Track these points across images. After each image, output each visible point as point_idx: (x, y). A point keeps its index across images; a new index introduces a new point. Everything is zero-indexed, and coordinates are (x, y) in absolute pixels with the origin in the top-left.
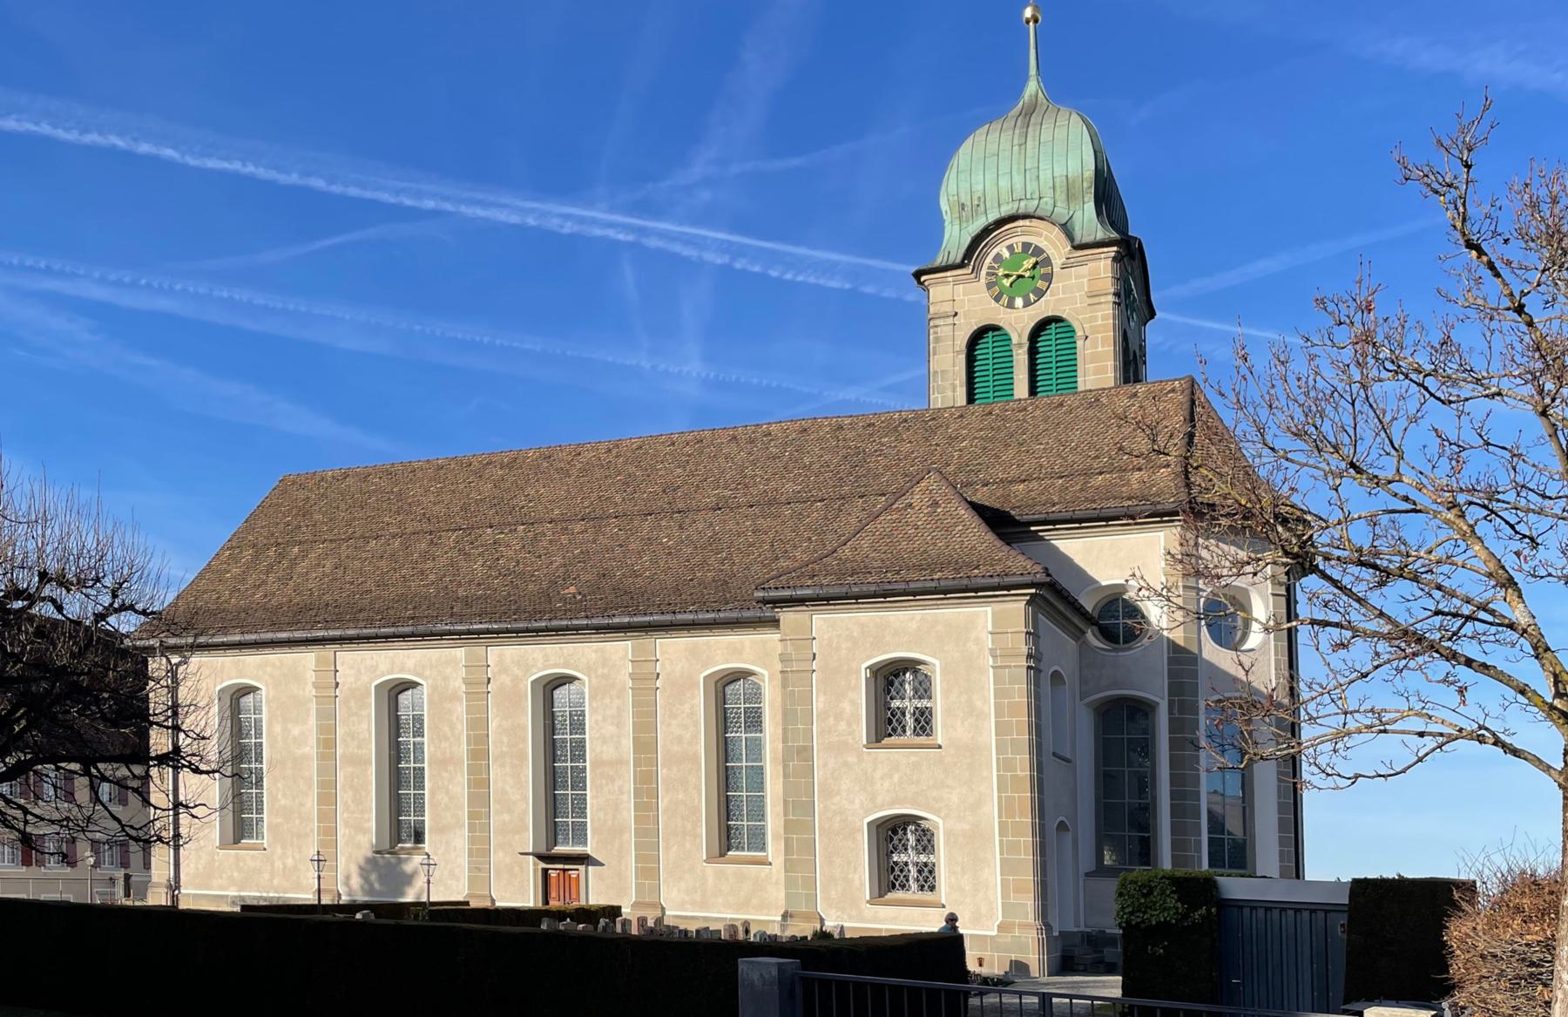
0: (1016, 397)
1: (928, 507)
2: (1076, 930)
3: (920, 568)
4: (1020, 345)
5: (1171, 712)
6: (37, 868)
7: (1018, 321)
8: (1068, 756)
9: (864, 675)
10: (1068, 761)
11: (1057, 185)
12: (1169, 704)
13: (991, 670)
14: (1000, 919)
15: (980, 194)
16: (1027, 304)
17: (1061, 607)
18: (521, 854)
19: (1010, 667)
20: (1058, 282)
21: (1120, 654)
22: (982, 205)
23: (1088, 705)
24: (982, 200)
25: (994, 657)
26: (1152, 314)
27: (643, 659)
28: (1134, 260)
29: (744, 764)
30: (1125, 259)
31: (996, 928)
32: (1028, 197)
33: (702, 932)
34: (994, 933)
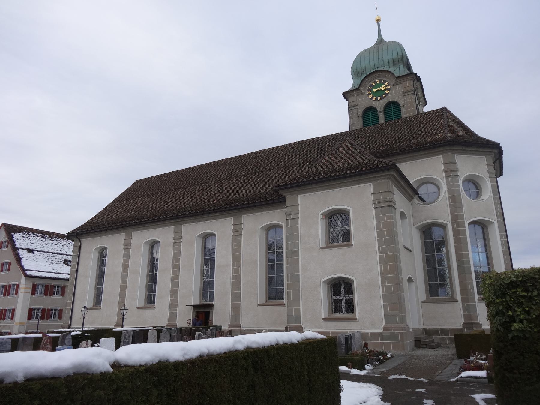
0: (380, 123)
1: (346, 151)
2: (419, 328)
3: (342, 170)
4: (381, 112)
5: (453, 227)
6: (47, 320)
7: (380, 105)
8: (410, 248)
9: (320, 217)
10: (410, 251)
11: (390, 61)
12: (452, 223)
13: (374, 210)
14: (384, 324)
15: (364, 68)
16: (382, 98)
17: (402, 183)
18: (187, 306)
19: (382, 207)
20: (392, 90)
21: (429, 205)
22: (365, 71)
23: (417, 228)
24: (365, 70)
25: (375, 204)
26: (426, 103)
27: (237, 224)
28: (418, 82)
29: (276, 263)
30: (415, 80)
31: (382, 328)
32: (380, 66)
33: (50, 347)
34: (382, 331)
